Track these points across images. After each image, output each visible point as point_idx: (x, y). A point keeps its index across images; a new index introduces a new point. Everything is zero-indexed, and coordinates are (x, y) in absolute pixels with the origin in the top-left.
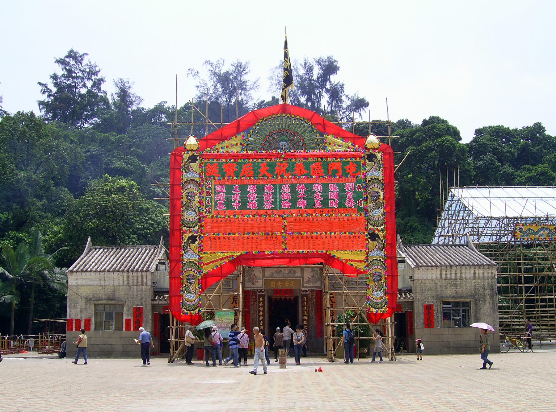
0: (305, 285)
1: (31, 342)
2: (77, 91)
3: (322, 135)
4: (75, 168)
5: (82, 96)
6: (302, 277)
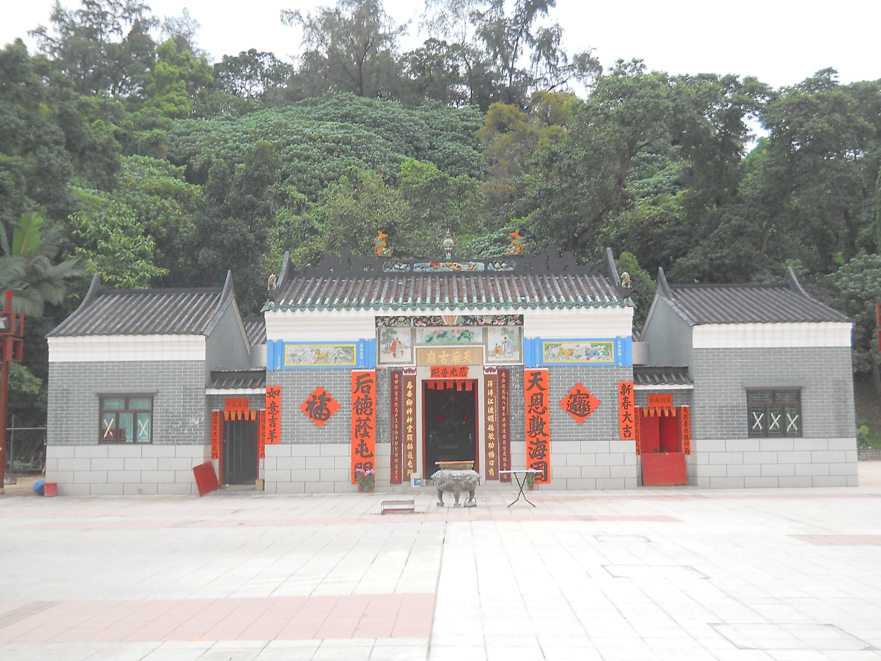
1: (784, 96)
2: (104, 37)
4: (80, 169)
5: (111, 48)
6: (485, 342)
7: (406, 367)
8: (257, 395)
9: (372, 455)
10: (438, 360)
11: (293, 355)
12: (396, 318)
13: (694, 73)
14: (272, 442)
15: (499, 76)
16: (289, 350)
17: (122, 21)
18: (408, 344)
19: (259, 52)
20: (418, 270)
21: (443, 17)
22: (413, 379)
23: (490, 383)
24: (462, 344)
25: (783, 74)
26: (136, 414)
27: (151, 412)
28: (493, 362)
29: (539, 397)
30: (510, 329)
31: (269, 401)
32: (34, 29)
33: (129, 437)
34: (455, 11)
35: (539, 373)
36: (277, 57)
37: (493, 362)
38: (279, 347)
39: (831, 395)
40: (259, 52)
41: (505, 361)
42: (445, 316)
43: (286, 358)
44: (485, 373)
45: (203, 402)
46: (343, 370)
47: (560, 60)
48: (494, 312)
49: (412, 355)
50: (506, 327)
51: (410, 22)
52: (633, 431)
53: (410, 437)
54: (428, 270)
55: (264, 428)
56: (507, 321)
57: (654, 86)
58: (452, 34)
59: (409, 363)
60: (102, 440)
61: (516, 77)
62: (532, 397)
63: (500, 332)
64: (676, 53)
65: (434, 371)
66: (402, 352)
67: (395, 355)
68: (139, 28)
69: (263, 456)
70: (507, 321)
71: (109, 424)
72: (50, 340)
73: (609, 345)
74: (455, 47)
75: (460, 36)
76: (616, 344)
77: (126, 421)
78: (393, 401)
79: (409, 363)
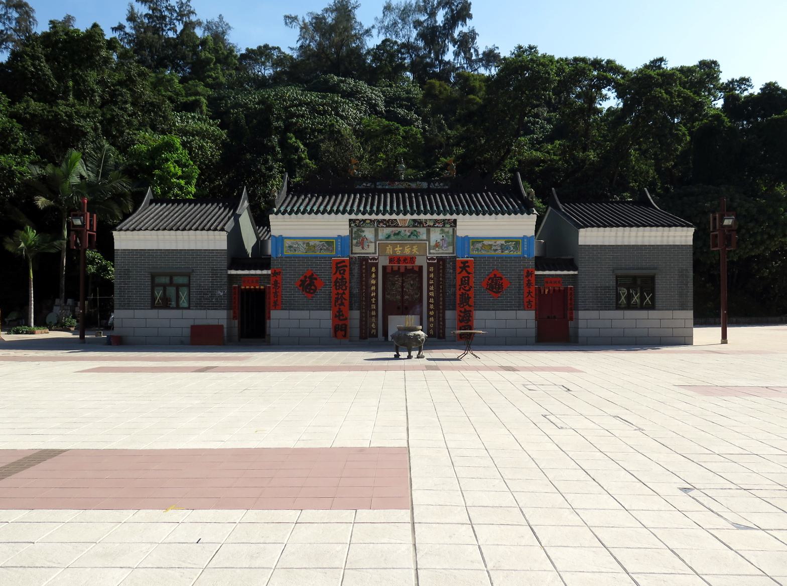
6: (428, 239)
7: (371, 256)
8: (264, 275)
9: (346, 319)
10: (394, 251)
11: (290, 247)
12: (364, 221)
13: (571, 56)
14: (275, 309)
15: (432, 65)
16: (287, 243)
17: (177, 23)
18: (373, 240)
19: (270, 46)
20: (380, 187)
21: (395, 24)
22: (376, 265)
23: (432, 269)
24: (412, 240)
25: (633, 61)
26: (178, 287)
27: (188, 285)
28: (434, 254)
29: (466, 279)
30: (446, 230)
31: (272, 279)
32: (116, 26)
33: (174, 304)
34: (403, 20)
35: (467, 262)
36: (283, 50)
37: (434, 254)
38: (280, 239)
39: (676, 281)
40: (270, 46)
41: (443, 253)
42: (399, 220)
43: (285, 249)
44: (428, 261)
45: (226, 280)
46: (325, 258)
47: (474, 55)
48: (435, 217)
49: (375, 247)
50: (444, 228)
51: (373, 27)
52: (533, 303)
53: (374, 307)
54: (387, 187)
55: (269, 298)
56: (444, 224)
57: (544, 65)
58: (401, 35)
59: (373, 253)
60: (153, 306)
61: (444, 66)
62: (462, 279)
63: (439, 232)
64: (562, 41)
65: (392, 260)
66: (368, 245)
67: (363, 248)
68: (189, 26)
69: (269, 318)
70: (444, 224)
71: (159, 294)
72: (115, 233)
73: (517, 242)
74: (404, 45)
75: (406, 37)
76: (523, 241)
77: (171, 291)
78: (361, 281)
79: (373, 253)
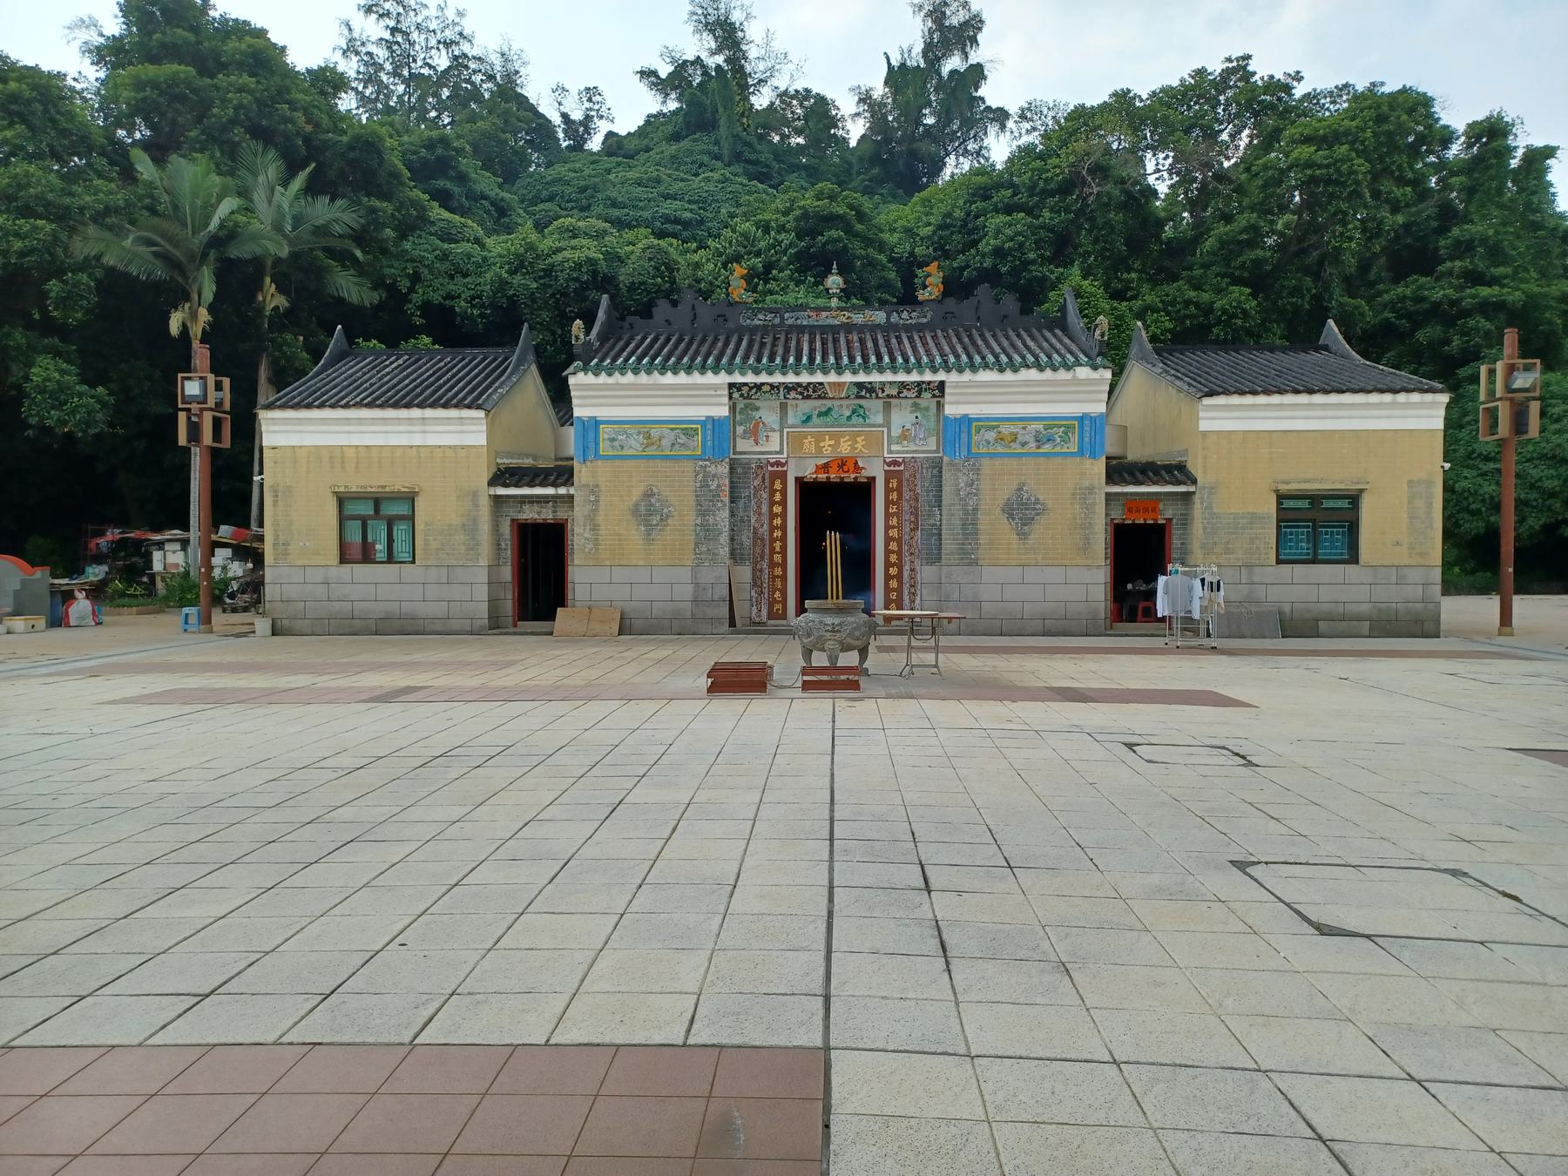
0: (894, 448)
3: (1217, 142)
